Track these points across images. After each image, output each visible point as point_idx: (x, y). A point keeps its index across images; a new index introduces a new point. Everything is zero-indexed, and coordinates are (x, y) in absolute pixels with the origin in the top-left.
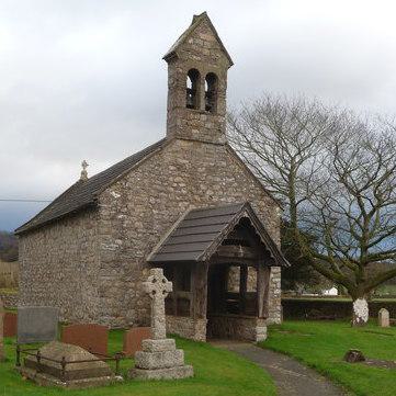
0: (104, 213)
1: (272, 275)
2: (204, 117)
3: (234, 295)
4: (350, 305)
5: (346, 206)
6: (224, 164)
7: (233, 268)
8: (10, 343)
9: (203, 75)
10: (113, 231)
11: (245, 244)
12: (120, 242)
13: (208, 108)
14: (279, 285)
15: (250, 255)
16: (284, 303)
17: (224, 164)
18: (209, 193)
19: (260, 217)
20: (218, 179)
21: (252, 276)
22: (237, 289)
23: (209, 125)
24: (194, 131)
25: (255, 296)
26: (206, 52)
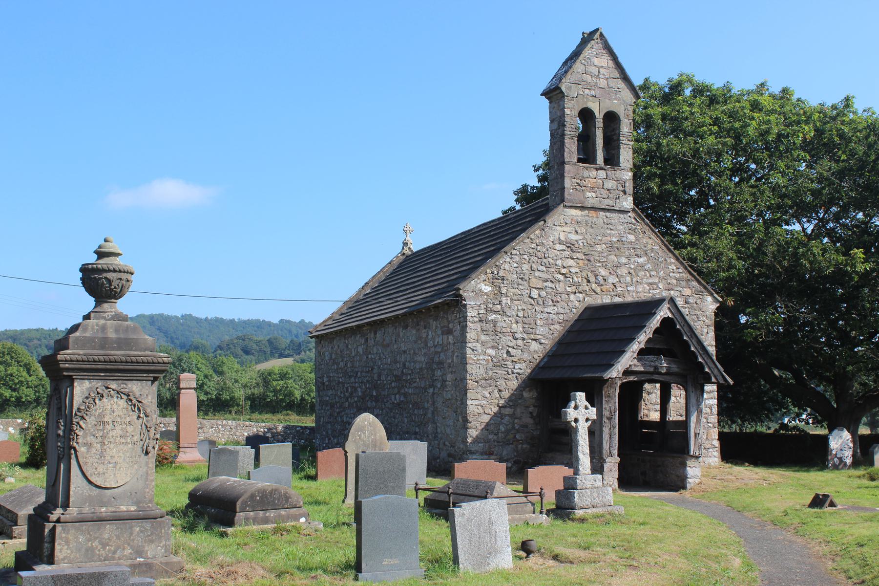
0: (471, 313)
1: (705, 396)
2: (602, 174)
3: (650, 424)
4: (824, 440)
5: (476, 410)
6: (632, 238)
7: (647, 386)
8: (303, 361)
9: (599, 116)
10: (483, 338)
11: (668, 354)
12: (492, 352)
13: (607, 161)
14: (715, 410)
15: (675, 368)
16: (722, 436)
17: (632, 238)
18: (612, 279)
19: (685, 311)
20: (624, 260)
21: (678, 396)
22: (655, 416)
23: (610, 184)
24: (589, 194)
25: (684, 425)
26: (603, 83)
